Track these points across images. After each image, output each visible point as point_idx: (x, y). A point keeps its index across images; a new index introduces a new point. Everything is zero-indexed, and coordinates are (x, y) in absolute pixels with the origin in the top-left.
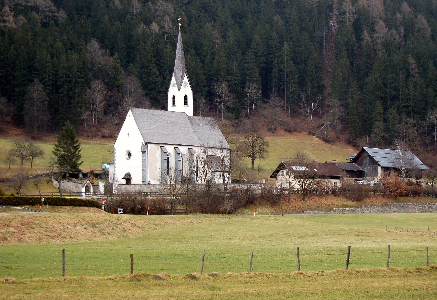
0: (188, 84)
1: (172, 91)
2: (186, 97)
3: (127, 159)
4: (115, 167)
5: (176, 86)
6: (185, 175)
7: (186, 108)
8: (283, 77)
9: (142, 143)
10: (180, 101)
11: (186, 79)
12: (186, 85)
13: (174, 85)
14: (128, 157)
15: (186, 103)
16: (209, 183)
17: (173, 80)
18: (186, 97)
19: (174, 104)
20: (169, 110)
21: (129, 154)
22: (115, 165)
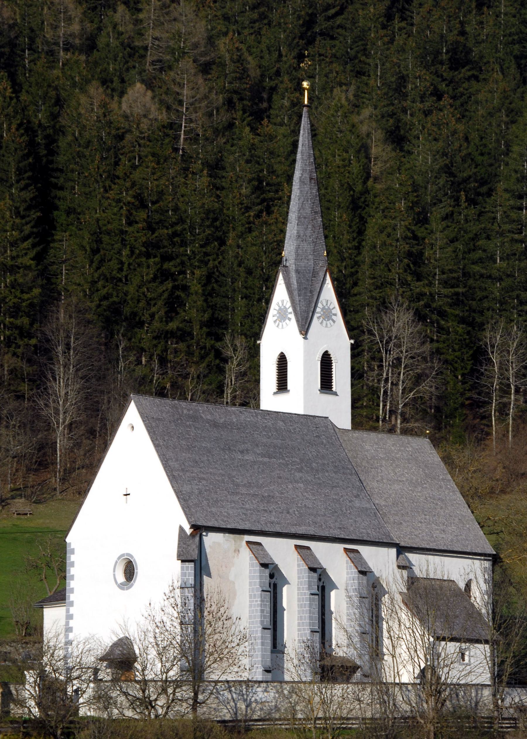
0: (337, 310)
1: (279, 335)
2: (326, 362)
3: (122, 586)
4: (69, 617)
5: (292, 316)
6: (109, 678)
7: (327, 398)
8: (333, 225)
9: (181, 529)
10: (303, 374)
11: (329, 294)
12: (328, 315)
13: (282, 316)
14: (121, 578)
15: (326, 384)
16: (429, 679)
17: (281, 295)
18: (326, 362)
19: (282, 385)
20: (264, 406)
21: (130, 571)
22: (72, 610)
